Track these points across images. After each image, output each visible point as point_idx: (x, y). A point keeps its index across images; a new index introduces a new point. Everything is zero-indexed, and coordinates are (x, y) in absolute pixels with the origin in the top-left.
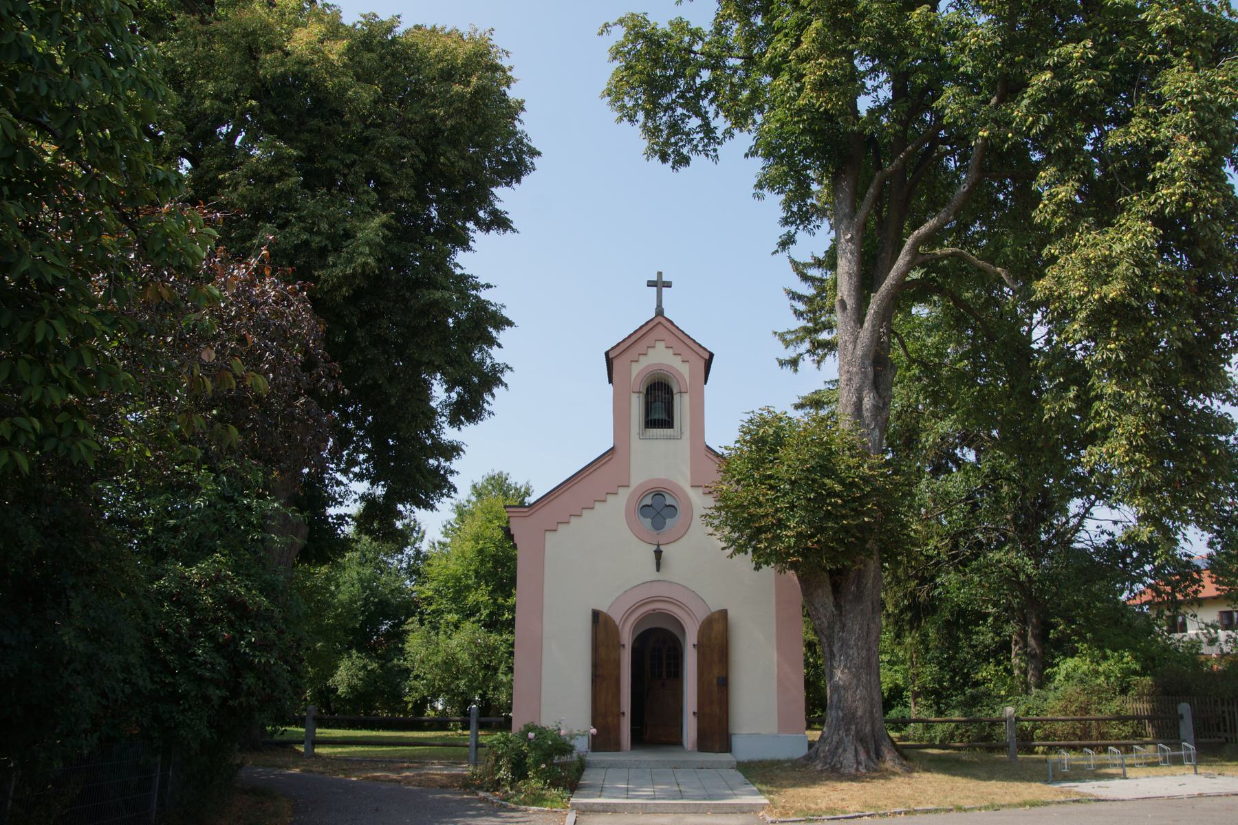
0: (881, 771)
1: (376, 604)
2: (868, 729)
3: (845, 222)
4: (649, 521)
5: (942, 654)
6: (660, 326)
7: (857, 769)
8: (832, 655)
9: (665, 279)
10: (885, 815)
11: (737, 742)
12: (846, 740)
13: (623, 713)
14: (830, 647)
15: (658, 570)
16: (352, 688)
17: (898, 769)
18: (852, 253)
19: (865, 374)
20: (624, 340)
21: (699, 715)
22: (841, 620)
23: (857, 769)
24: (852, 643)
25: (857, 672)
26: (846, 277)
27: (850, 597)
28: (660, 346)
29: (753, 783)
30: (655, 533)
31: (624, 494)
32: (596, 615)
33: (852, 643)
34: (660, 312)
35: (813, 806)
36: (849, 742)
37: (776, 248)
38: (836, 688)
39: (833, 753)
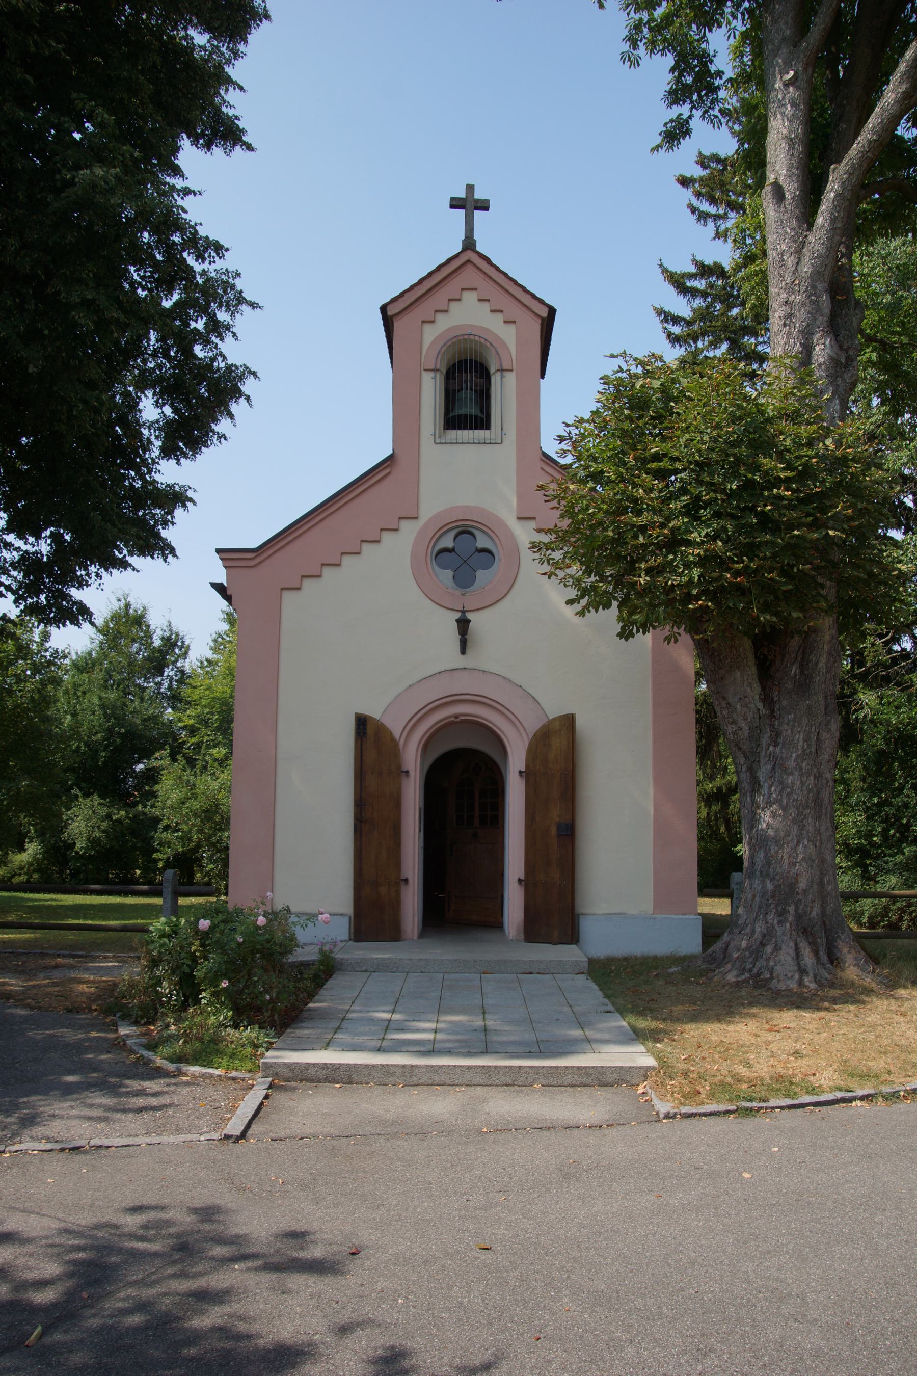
0: (842, 986)
1: (123, 736)
2: (815, 911)
3: (784, 51)
4: (450, 573)
5: (871, 798)
6: (470, 268)
7: (800, 983)
8: (756, 786)
9: (477, 196)
10: (895, 1095)
11: (589, 928)
12: (779, 930)
13: (406, 881)
14: (752, 771)
15: (463, 651)
16: (93, 842)
17: (868, 981)
18: (794, 104)
19: (816, 303)
20: (412, 288)
21: (528, 883)
22: (772, 726)
23: (800, 983)
24: (792, 763)
25: (799, 814)
26: (784, 145)
27: (789, 686)
28: (470, 298)
29: (622, 1012)
30: (458, 592)
31: (409, 531)
32: (362, 722)
33: (792, 763)
34: (469, 244)
35: (743, 1071)
36: (784, 931)
37: (658, 140)
38: (760, 842)
39: (757, 952)
